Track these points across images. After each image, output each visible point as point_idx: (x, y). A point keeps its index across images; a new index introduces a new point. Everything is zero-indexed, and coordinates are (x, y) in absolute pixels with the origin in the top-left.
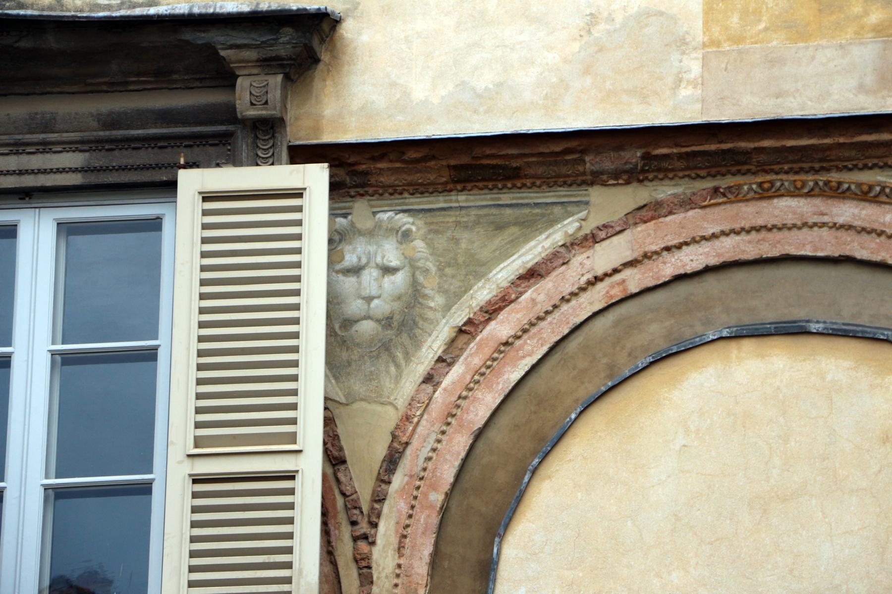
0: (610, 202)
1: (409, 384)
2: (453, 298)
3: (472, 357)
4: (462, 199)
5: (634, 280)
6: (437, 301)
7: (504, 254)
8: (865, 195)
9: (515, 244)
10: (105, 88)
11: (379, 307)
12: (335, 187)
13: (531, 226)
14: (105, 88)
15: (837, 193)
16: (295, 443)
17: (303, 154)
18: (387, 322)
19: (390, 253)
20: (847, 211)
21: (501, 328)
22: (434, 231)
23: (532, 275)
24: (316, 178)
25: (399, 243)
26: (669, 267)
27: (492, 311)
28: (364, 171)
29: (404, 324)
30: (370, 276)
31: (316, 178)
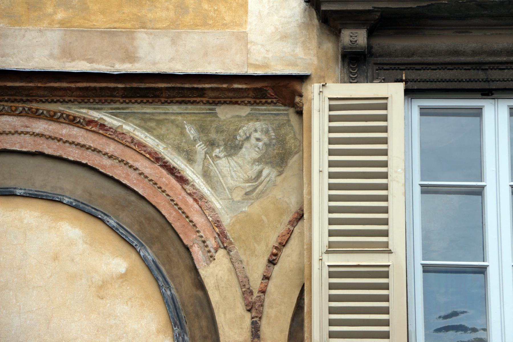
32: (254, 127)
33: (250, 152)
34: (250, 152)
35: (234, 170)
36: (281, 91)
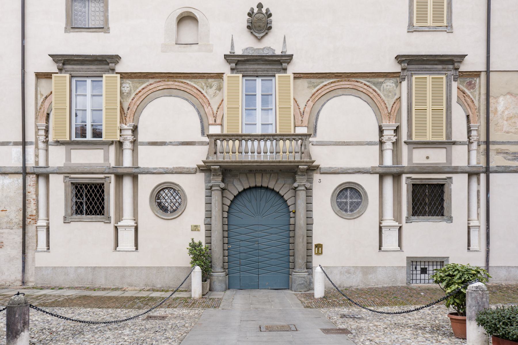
0: (151, 81)
1: (130, 100)
2: (135, 91)
3: (137, 97)
4: (135, 80)
5: (155, 90)
6: (133, 91)
7: (140, 86)
8: (178, 82)
9: (141, 85)
10: (302, 75)
11: (127, 91)
12: (121, 78)
13: (143, 83)
14: (302, 75)
15: (175, 81)
16: (85, 137)
17: (117, 73)
18: (128, 93)
19: (128, 85)
20: (176, 83)
21: (140, 94)
22: (133, 83)
23: (143, 89)
24: (119, 75)
25: (128, 85)
26: (158, 88)
27: (140, 92)
28: (125, 76)
29: (129, 93)
30: (126, 88)
31: (119, 75)
32: (214, 83)
33: (214, 88)
34: (214, 88)
35: (212, 91)
36: (219, 76)
